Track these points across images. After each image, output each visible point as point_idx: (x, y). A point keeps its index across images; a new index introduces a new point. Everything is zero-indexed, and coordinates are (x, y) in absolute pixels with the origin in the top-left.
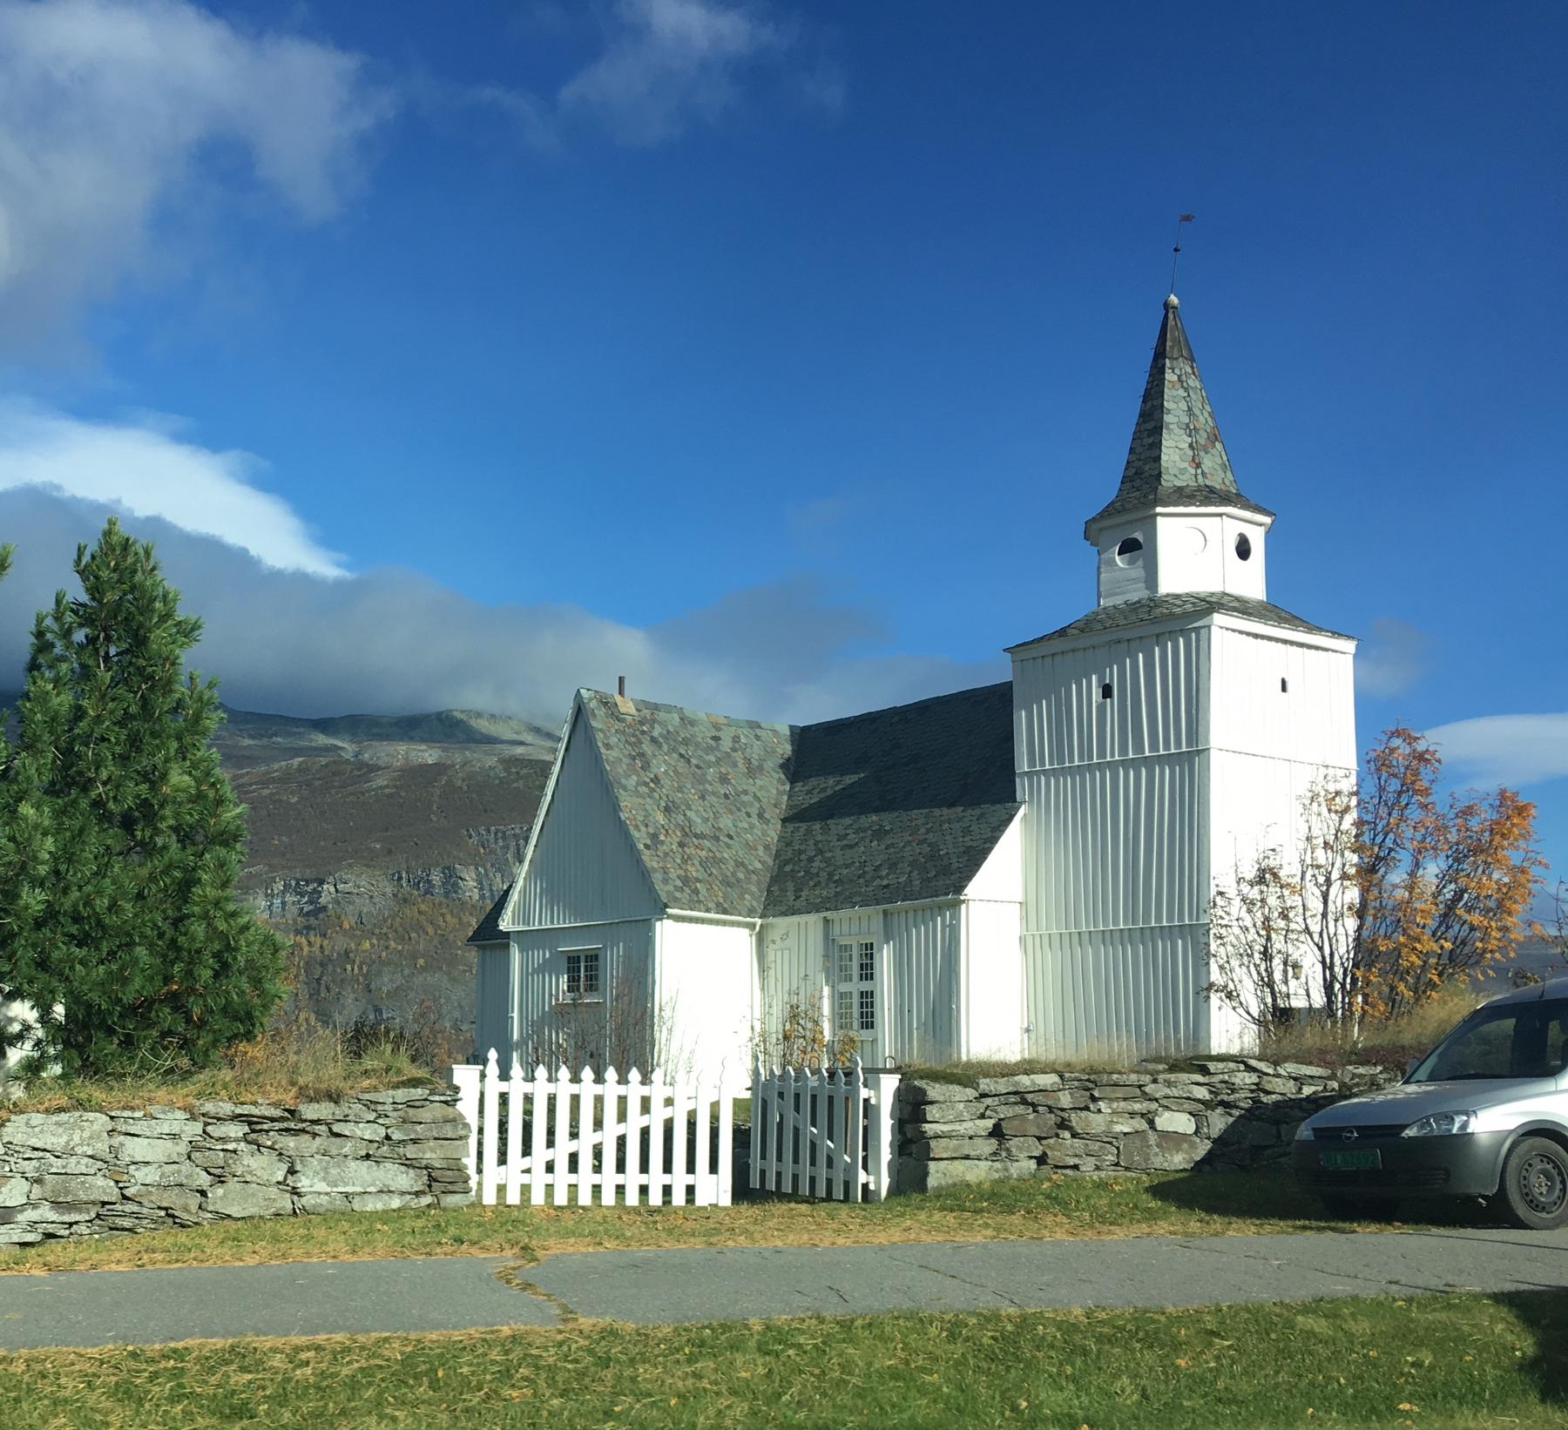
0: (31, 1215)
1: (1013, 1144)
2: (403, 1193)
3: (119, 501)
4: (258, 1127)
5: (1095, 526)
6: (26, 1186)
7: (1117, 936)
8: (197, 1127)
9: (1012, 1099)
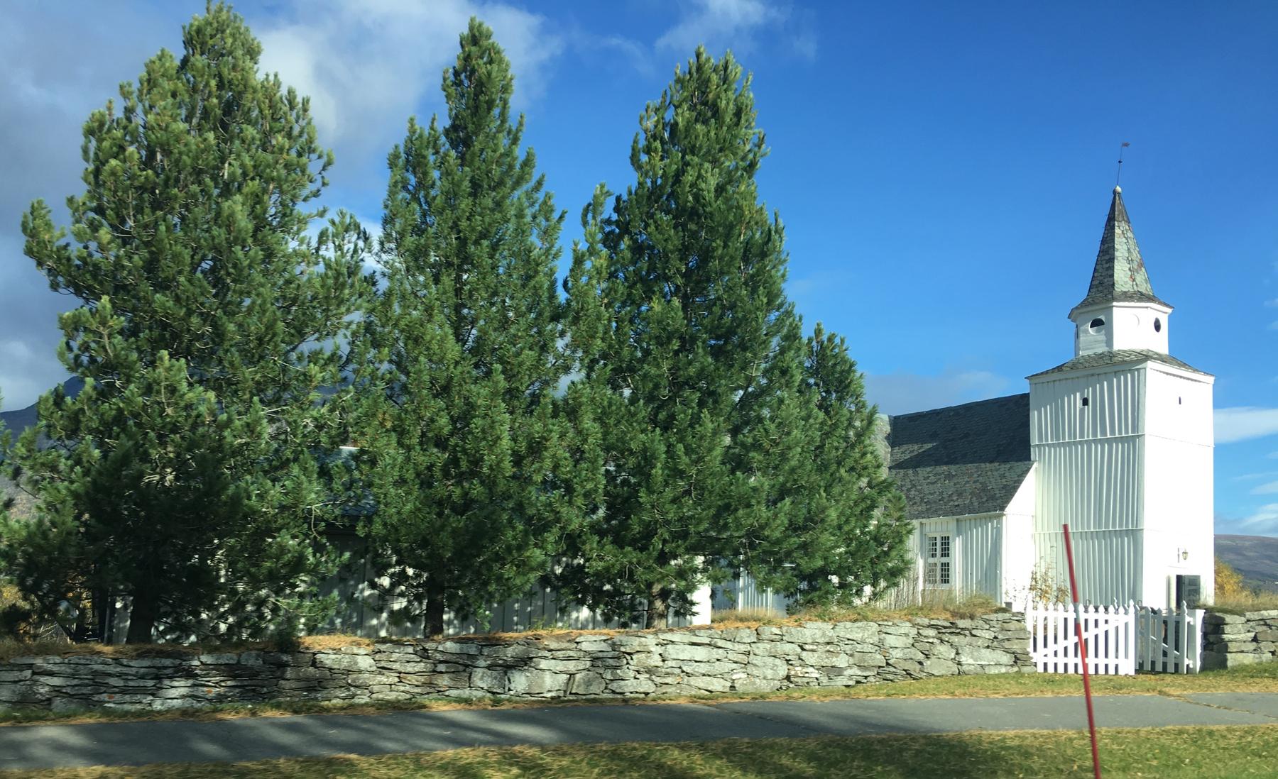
0: (849, 672)
1: (1262, 645)
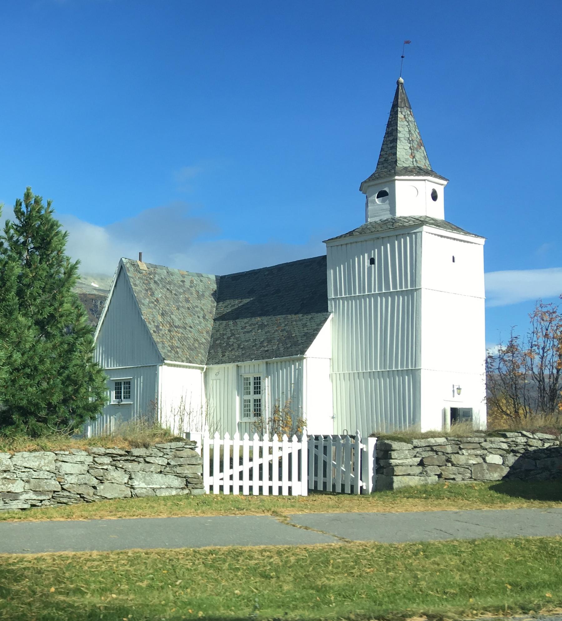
0: (25, 496)
1: (428, 469)
2: (176, 488)
4: (116, 459)
5: (365, 185)
6: (23, 483)
7: (376, 374)
8: (90, 459)
9: (428, 449)
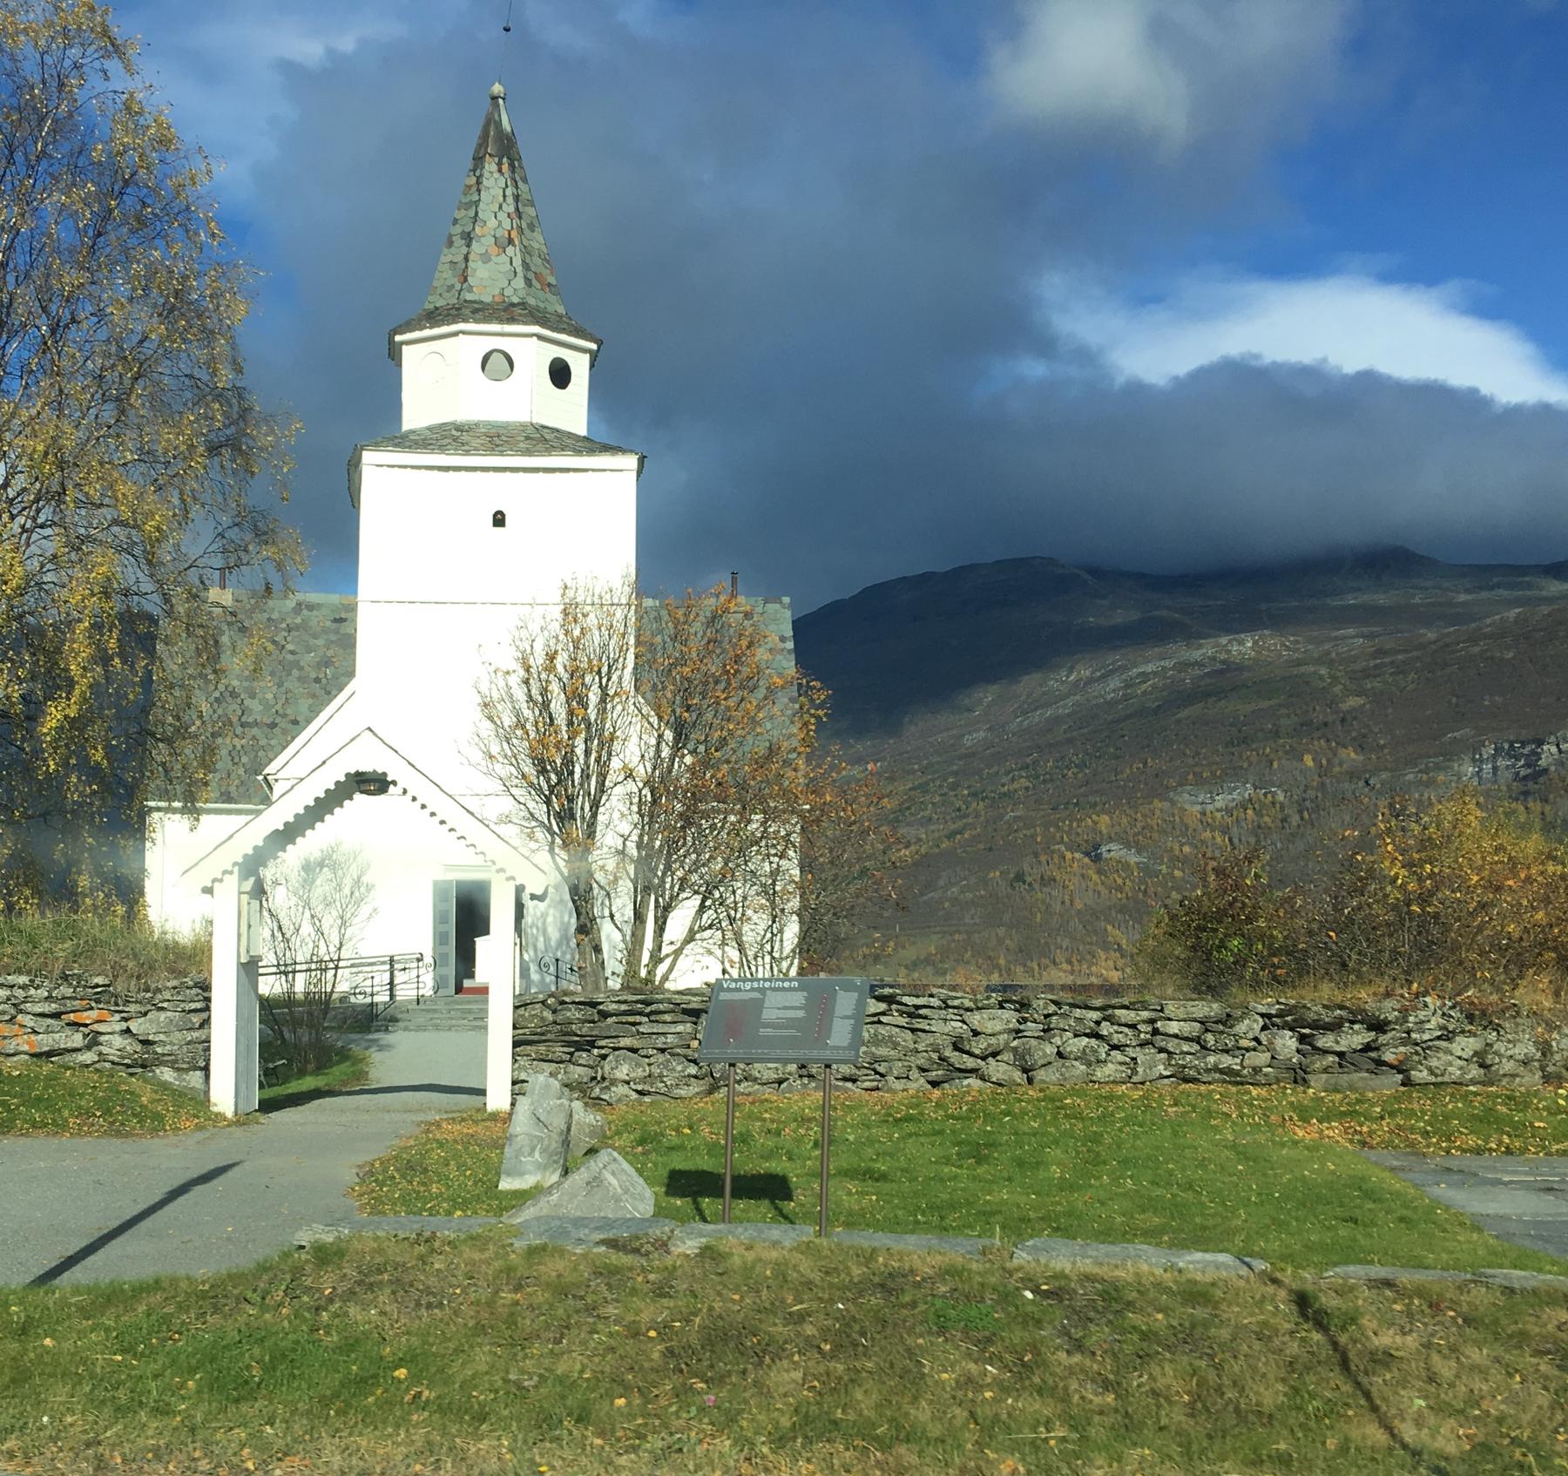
3: (1325, 360)
